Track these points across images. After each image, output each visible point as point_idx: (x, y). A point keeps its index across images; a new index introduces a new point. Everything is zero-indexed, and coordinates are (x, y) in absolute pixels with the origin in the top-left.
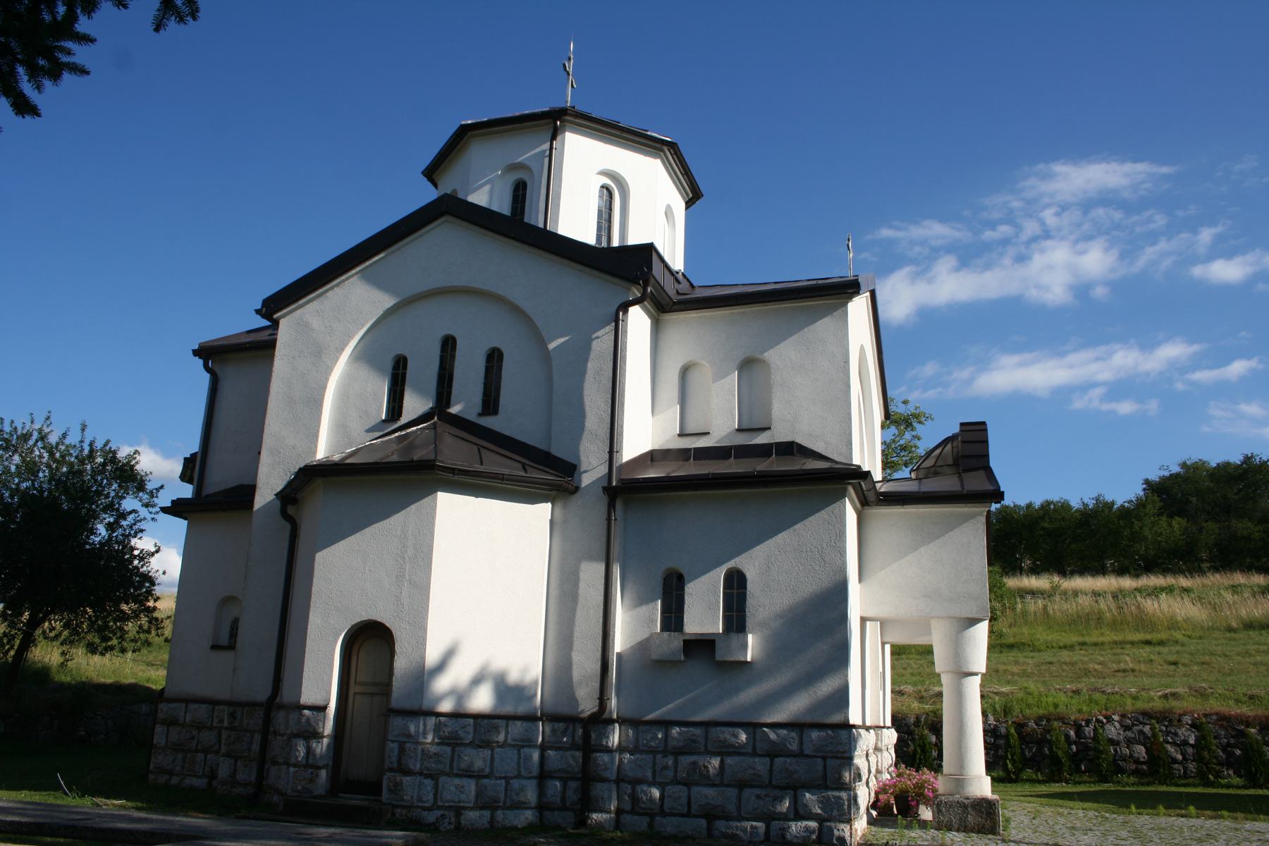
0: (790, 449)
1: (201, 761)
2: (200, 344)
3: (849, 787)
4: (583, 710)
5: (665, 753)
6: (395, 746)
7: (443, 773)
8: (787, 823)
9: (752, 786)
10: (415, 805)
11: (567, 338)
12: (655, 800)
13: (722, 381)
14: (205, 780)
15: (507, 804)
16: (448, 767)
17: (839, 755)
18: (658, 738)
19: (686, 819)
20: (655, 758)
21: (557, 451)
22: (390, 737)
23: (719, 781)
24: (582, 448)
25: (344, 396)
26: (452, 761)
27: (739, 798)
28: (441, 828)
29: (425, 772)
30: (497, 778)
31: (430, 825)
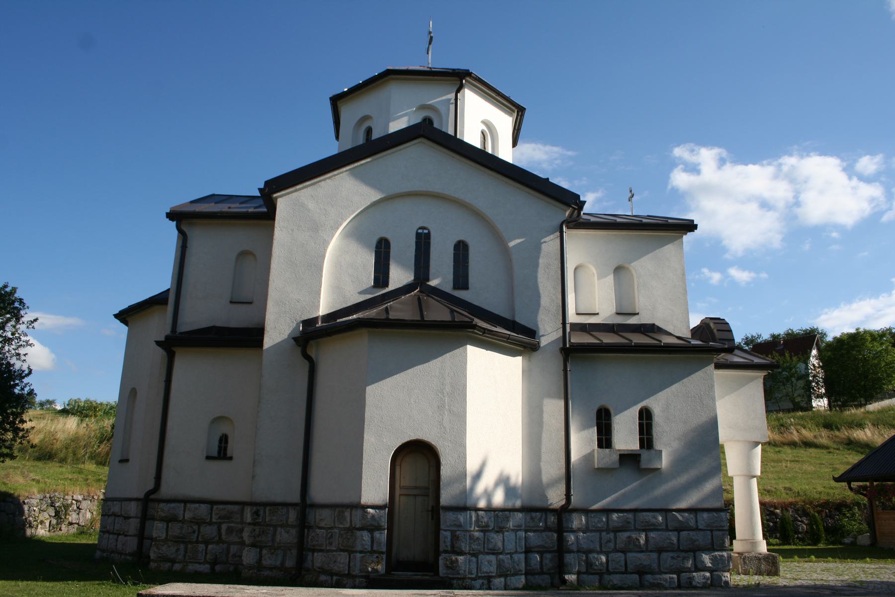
0: (650, 329)
1: (203, 550)
4: (552, 503)
5: (608, 531)
6: (448, 534)
9: (667, 551)
11: (522, 240)
14: (208, 566)
17: (721, 529)
18: (603, 521)
19: (625, 575)
20: (601, 535)
21: (522, 319)
22: (442, 527)
23: (645, 550)
24: (539, 319)
25: (337, 265)
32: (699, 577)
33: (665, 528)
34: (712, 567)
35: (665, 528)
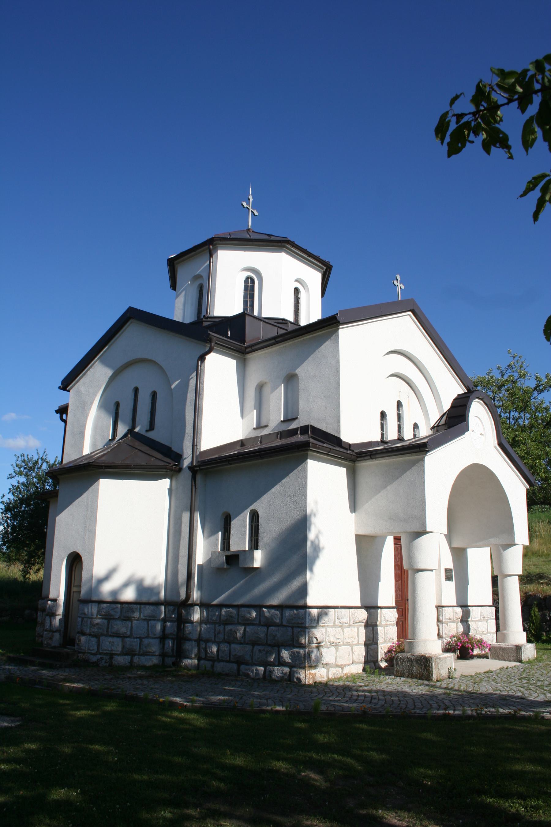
2: (59, 407)
3: (304, 645)
7: (103, 635)
8: (273, 667)
9: (259, 645)
10: (87, 652)
11: (179, 381)
12: (213, 652)
13: (276, 391)
15: (141, 653)
16: (105, 631)
17: (300, 625)
23: (243, 642)
25: (95, 428)
26: (108, 628)
27: (252, 651)
28: (100, 665)
29: (92, 634)
30: (134, 638)
31: (93, 663)
32: (278, 671)
33: (258, 623)
34: (292, 662)
35: (258, 623)
